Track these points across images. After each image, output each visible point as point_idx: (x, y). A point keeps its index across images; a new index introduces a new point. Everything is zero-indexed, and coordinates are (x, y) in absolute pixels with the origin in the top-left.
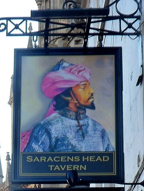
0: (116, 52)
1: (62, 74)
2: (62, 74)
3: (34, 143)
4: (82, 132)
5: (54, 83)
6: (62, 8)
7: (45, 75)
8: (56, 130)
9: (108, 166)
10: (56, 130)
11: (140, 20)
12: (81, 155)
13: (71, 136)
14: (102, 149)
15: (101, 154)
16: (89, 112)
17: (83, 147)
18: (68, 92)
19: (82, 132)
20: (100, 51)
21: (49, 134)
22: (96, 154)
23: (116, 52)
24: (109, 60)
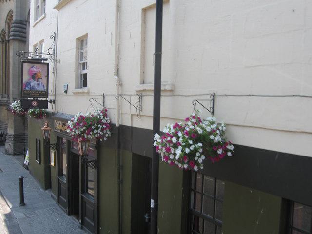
0: (48, 64)
1: (34, 69)
2: (34, 69)
3: (29, 58)
4: (38, 85)
5: (32, 71)
6: (93, 183)
7: (29, 69)
8: (32, 84)
9: (44, 94)
10: (32, 84)
11: (294, 202)
12: (38, 91)
13: (36, 86)
14: (43, 90)
15: (43, 91)
16: (40, 80)
17: (39, 89)
18: (35, 74)
19: (38, 85)
20: (44, 64)
21: (30, 85)
22: (42, 91)
23: (48, 64)
24: (46, 66)
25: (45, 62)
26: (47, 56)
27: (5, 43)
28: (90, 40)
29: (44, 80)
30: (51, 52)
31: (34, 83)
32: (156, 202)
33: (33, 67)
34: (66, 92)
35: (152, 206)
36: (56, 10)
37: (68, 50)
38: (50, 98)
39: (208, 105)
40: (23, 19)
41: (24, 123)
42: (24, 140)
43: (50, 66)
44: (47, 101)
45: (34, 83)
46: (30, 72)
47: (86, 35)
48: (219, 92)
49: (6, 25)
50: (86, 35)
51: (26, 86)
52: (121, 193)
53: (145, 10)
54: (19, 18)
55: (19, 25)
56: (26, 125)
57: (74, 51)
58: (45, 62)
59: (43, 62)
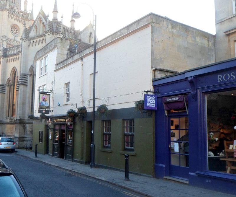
0: (50, 95)
1: (44, 97)
2: (44, 97)
4: (46, 103)
18: (45, 99)
19: (46, 103)
23: (50, 95)
24: (49, 95)
25: (49, 94)
26: (49, 91)
27: (9, 86)
28: (70, 84)
29: (48, 102)
30: (51, 89)
31: (44, 103)
32: (94, 131)
33: (44, 96)
34: (59, 105)
35: (92, 133)
36: (54, 72)
37: (60, 89)
38: (51, 109)
39: (107, 100)
40: (26, 73)
41: (24, 131)
42: (24, 140)
43: (51, 95)
44: (49, 111)
45: (44, 103)
46: (42, 98)
47: (69, 83)
48: (109, 97)
49: (11, 75)
50: (69, 83)
51: (41, 104)
52: (94, 22)
53: (91, 74)
54: (24, 73)
55: (24, 76)
56: (26, 132)
57: (64, 89)
58: (49, 94)
59: (47, 93)
